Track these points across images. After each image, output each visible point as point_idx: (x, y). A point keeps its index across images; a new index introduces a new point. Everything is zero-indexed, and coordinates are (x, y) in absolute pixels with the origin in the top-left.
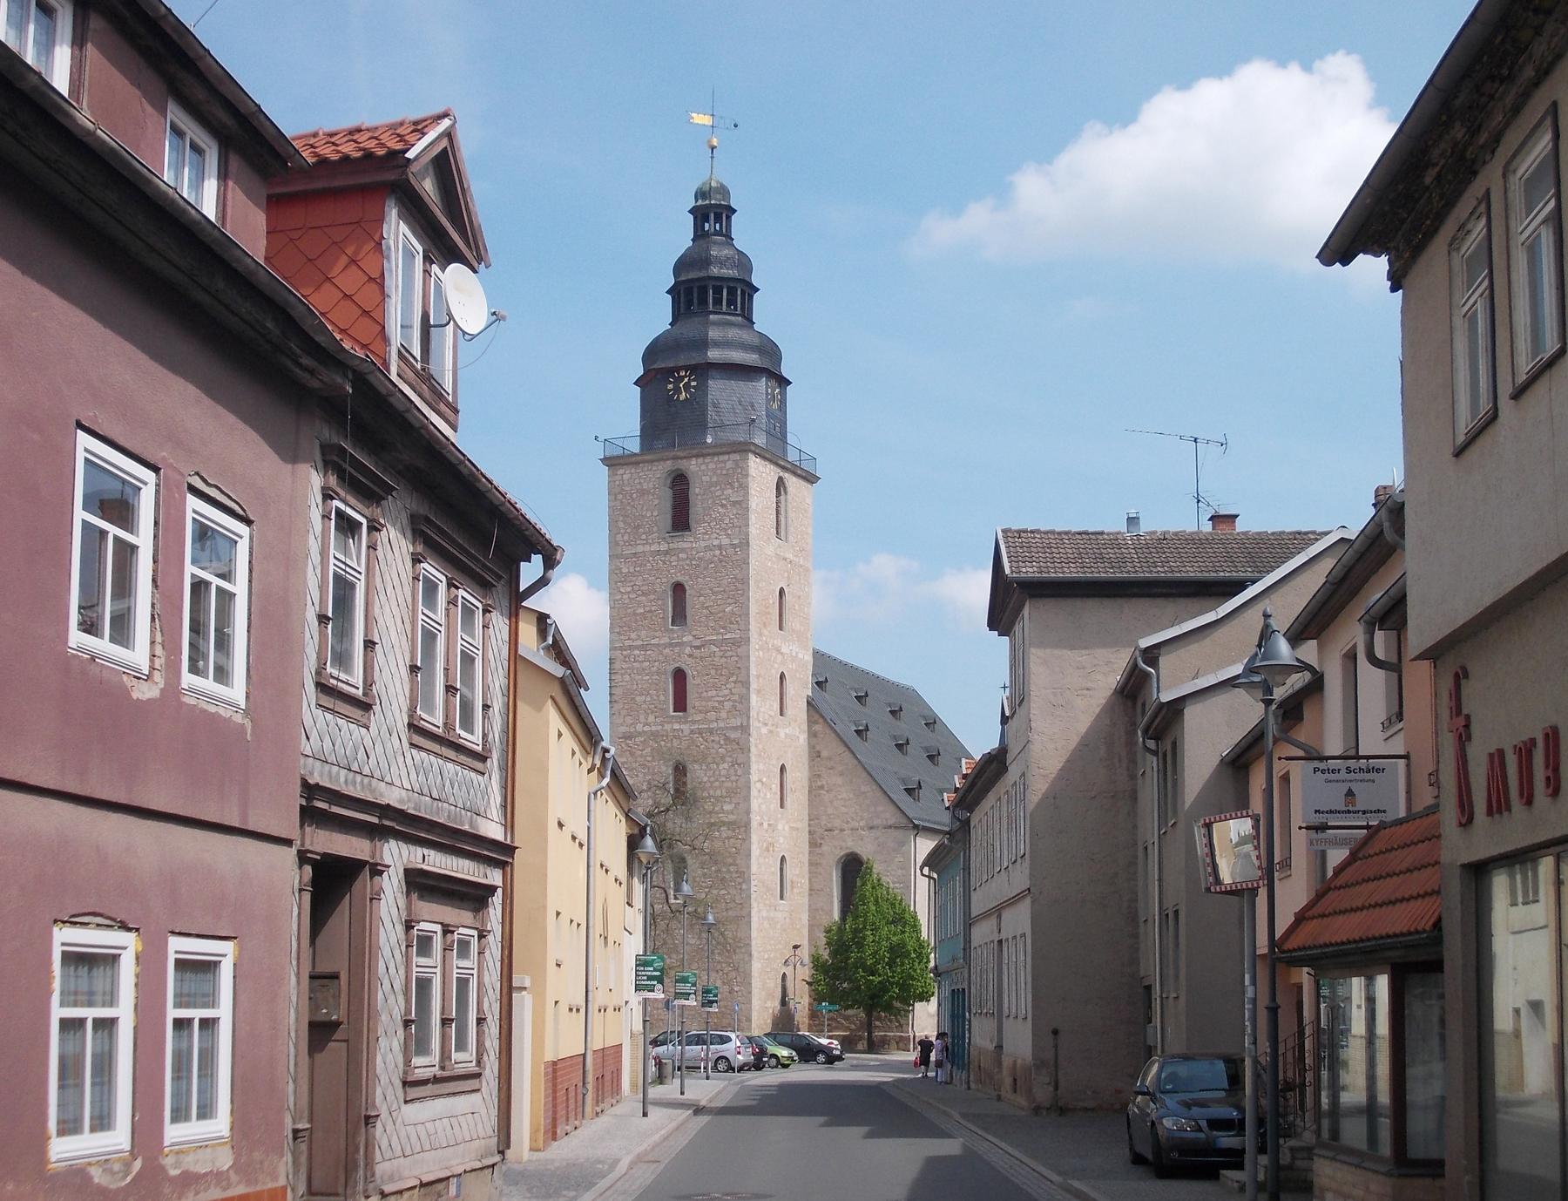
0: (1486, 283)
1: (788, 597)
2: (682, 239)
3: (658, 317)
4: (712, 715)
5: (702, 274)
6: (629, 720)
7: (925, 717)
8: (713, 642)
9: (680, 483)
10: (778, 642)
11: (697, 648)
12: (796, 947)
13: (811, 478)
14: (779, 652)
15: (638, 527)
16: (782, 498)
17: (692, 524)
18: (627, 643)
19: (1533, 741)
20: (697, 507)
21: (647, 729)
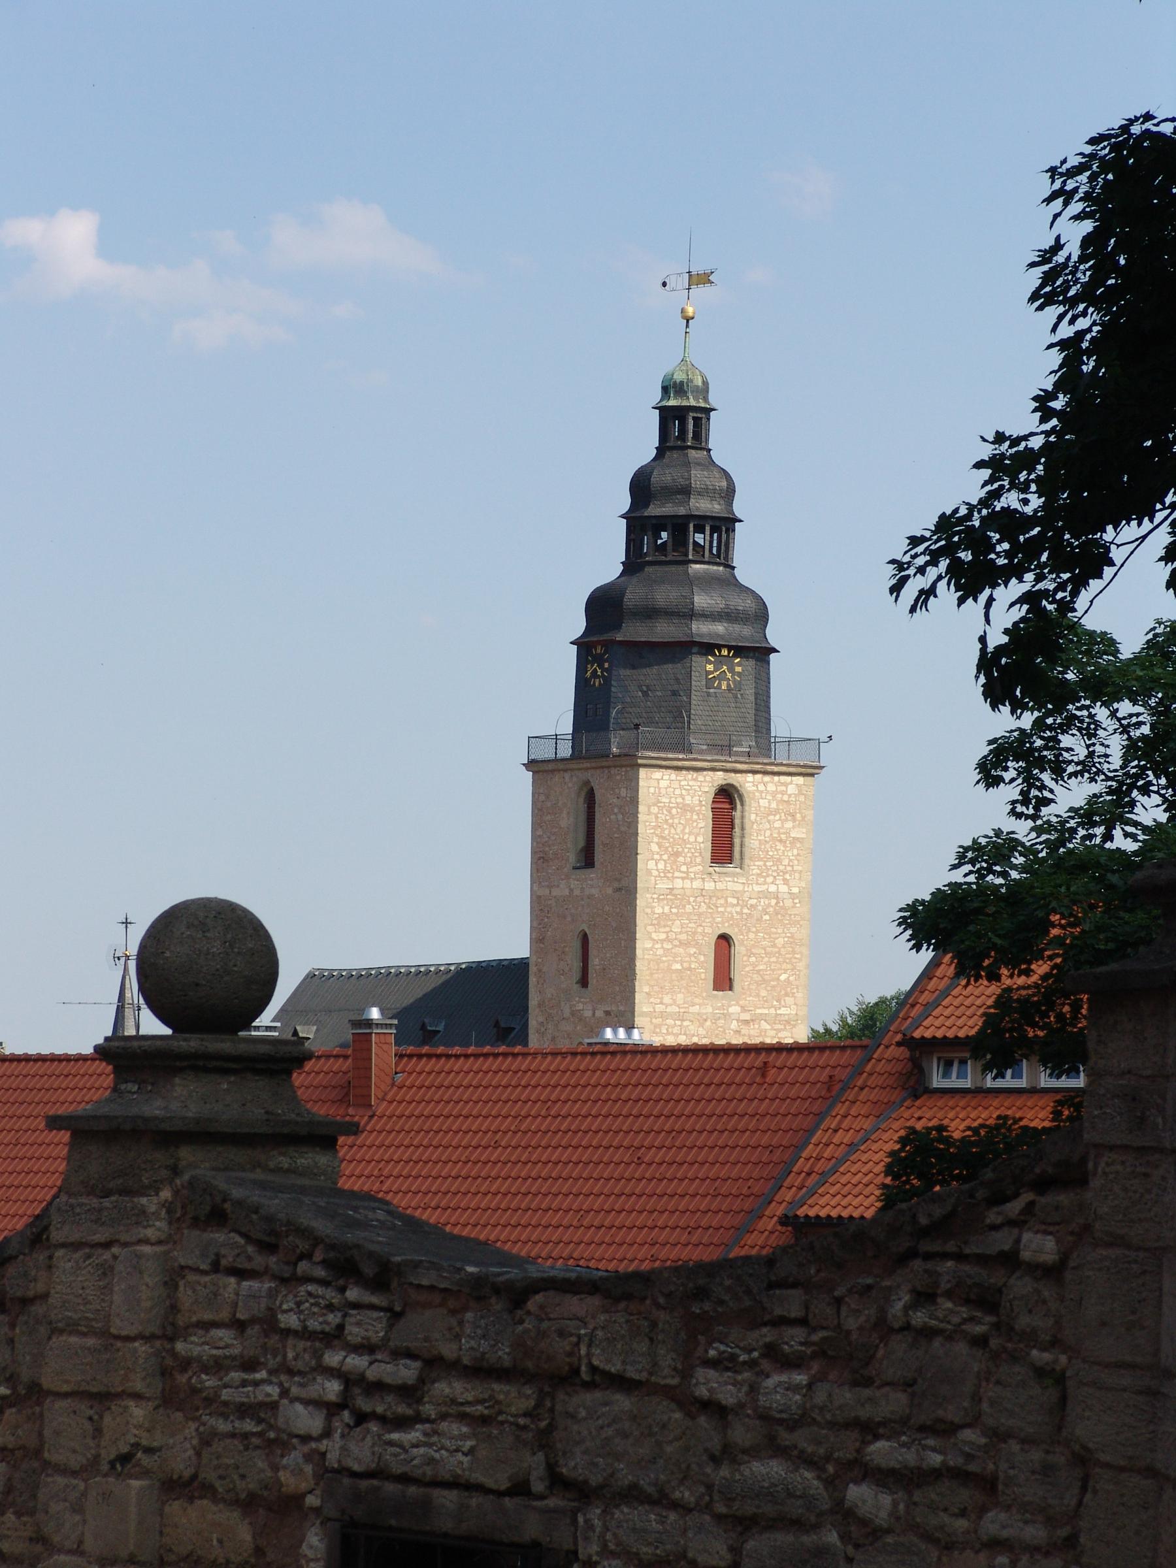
2: (643, 444)
5: (682, 511)
8: (764, 1018)
11: (746, 1022)
15: (677, 854)
18: (659, 1008)
19: (1155, 118)
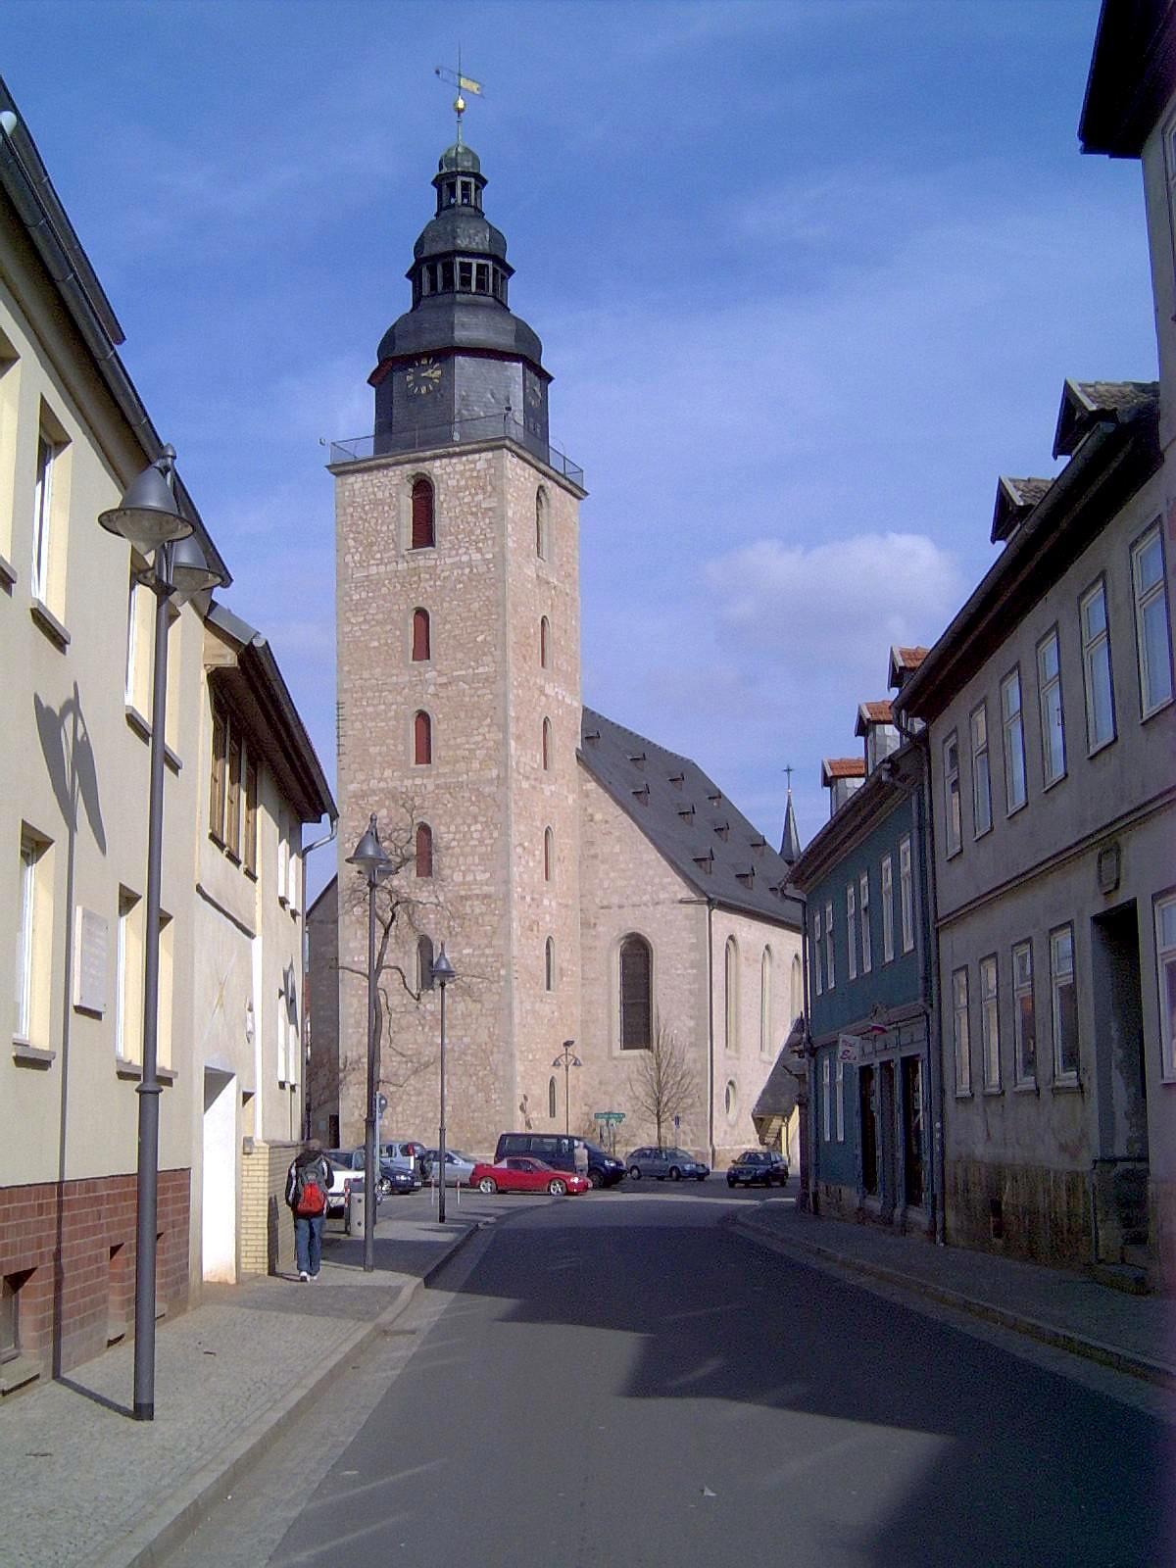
0: (1162, 583)
1: (550, 629)
3: (393, 299)
4: (461, 766)
6: (361, 776)
7: (707, 791)
8: (463, 679)
9: (423, 489)
10: (540, 681)
11: (443, 685)
12: (567, 1044)
13: (577, 492)
14: (542, 692)
15: (372, 544)
16: (544, 511)
17: (438, 538)
20: (442, 519)
21: (382, 785)
